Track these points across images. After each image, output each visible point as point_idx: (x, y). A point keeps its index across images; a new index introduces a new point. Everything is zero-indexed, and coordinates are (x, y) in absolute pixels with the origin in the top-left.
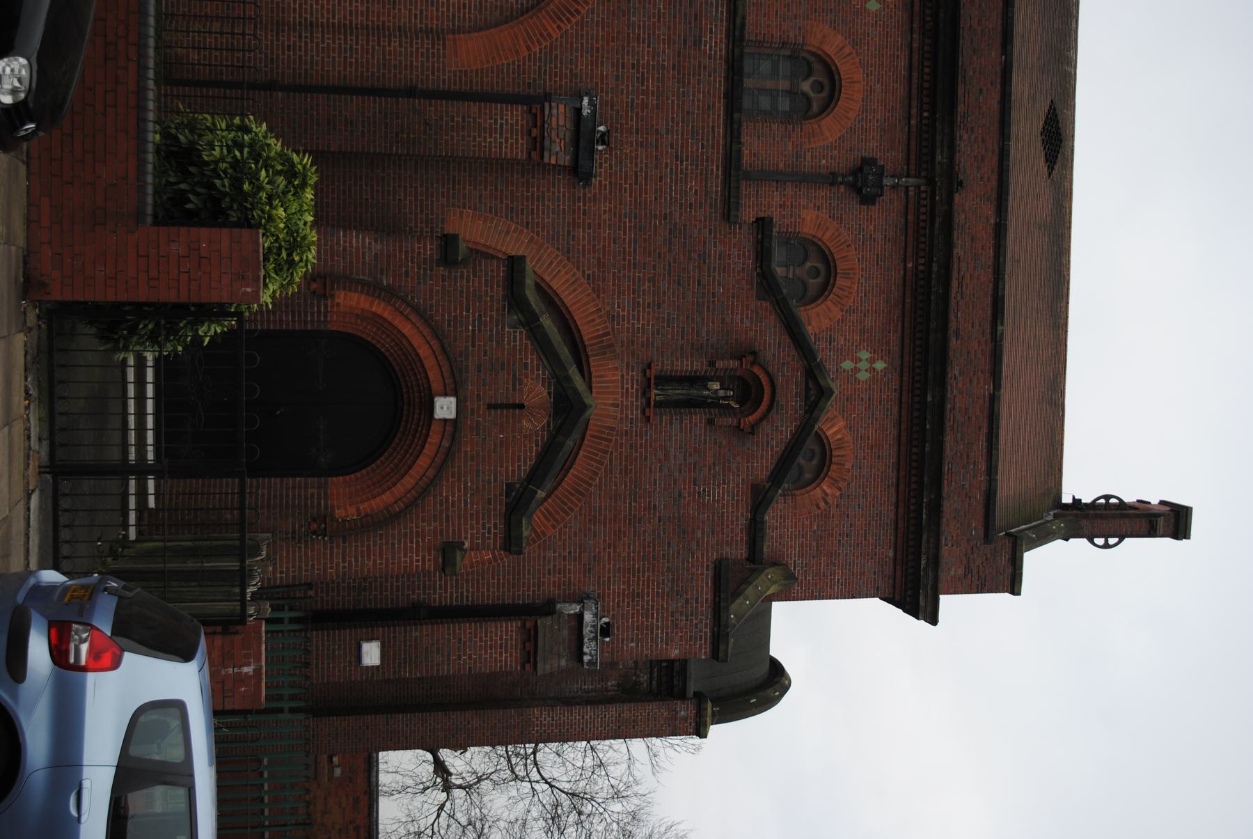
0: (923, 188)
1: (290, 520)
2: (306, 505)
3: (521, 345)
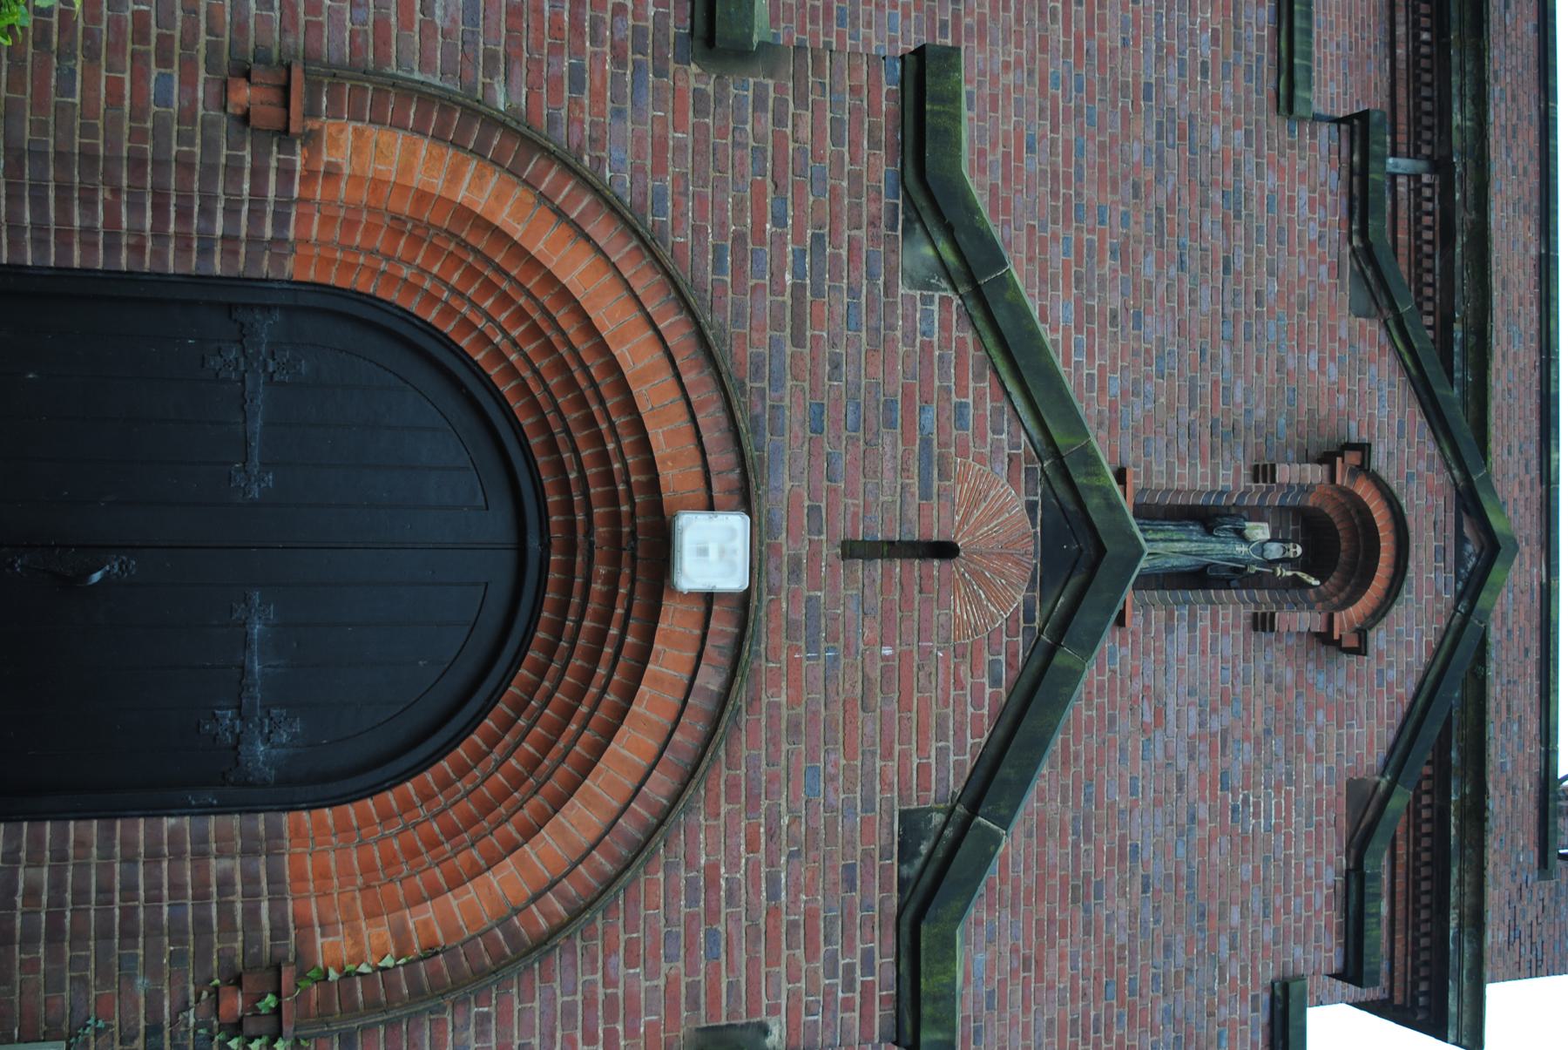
0: (1426, 179)
1: (141, 983)
2: (202, 924)
3: (945, 343)
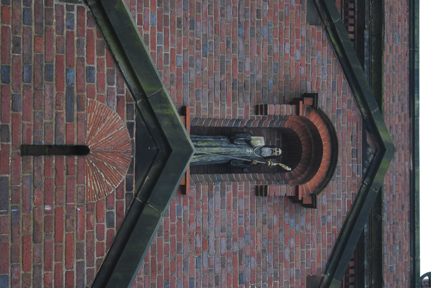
3: (81, 33)
